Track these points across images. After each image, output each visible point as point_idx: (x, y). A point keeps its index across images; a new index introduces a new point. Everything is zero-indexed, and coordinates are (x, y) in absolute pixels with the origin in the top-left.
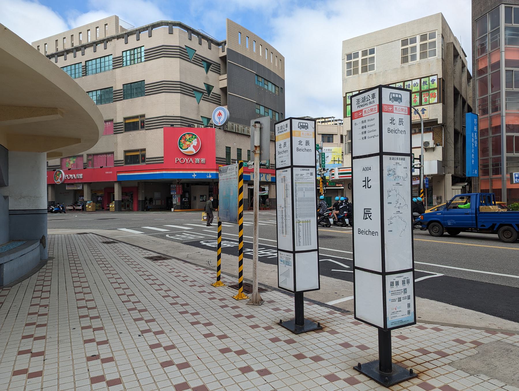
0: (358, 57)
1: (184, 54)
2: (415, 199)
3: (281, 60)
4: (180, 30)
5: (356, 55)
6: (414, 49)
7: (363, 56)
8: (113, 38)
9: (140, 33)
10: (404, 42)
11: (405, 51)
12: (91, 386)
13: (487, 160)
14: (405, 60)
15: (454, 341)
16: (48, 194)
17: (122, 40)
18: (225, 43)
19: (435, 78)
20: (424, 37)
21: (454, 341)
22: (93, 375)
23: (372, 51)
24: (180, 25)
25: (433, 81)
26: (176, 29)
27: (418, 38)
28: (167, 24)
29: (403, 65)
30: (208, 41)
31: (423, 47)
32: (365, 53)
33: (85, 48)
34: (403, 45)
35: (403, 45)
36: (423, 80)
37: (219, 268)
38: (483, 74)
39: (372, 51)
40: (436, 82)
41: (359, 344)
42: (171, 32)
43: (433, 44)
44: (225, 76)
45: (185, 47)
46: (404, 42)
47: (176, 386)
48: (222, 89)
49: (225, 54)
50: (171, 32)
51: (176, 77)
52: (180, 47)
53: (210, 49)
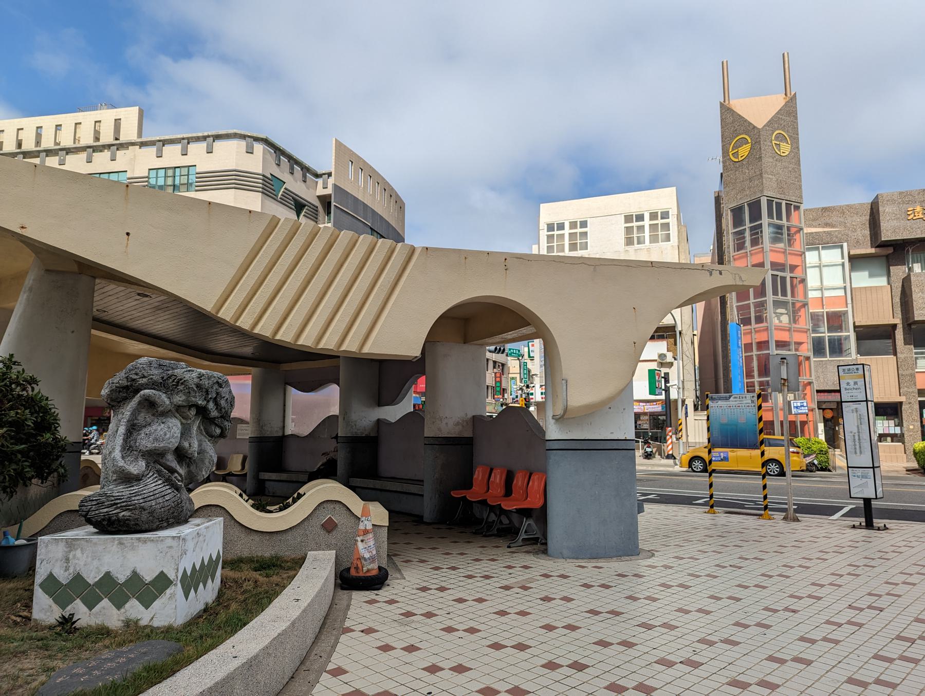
0: (563, 229)
1: (270, 187)
2: (751, 290)
3: (400, 206)
4: (264, 149)
5: (561, 226)
6: (641, 229)
7: (571, 228)
8: (133, 144)
9: (188, 143)
10: (628, 218)
11: (629, 230)
13: (748, 306)
17: (153, 150)
18: (330, 175)
20: (653, 216)
23: (584, 224)
24: (266, 141)
26: (259, 148)
28: (243, 137)
29: (628, 248)
30: (302, 169)
31: (653, 227)
32: (573, 225)
33: (67, 154)
34: (626, 222)
38: (824, 345)
39: (584, 224)
41: (544, 662)
42: (250, 151)
43: (666, 226)
45: (270, 176)
46: (628, 218)
49: (329, 191)
50: (250, 151)
52: (263, 176)
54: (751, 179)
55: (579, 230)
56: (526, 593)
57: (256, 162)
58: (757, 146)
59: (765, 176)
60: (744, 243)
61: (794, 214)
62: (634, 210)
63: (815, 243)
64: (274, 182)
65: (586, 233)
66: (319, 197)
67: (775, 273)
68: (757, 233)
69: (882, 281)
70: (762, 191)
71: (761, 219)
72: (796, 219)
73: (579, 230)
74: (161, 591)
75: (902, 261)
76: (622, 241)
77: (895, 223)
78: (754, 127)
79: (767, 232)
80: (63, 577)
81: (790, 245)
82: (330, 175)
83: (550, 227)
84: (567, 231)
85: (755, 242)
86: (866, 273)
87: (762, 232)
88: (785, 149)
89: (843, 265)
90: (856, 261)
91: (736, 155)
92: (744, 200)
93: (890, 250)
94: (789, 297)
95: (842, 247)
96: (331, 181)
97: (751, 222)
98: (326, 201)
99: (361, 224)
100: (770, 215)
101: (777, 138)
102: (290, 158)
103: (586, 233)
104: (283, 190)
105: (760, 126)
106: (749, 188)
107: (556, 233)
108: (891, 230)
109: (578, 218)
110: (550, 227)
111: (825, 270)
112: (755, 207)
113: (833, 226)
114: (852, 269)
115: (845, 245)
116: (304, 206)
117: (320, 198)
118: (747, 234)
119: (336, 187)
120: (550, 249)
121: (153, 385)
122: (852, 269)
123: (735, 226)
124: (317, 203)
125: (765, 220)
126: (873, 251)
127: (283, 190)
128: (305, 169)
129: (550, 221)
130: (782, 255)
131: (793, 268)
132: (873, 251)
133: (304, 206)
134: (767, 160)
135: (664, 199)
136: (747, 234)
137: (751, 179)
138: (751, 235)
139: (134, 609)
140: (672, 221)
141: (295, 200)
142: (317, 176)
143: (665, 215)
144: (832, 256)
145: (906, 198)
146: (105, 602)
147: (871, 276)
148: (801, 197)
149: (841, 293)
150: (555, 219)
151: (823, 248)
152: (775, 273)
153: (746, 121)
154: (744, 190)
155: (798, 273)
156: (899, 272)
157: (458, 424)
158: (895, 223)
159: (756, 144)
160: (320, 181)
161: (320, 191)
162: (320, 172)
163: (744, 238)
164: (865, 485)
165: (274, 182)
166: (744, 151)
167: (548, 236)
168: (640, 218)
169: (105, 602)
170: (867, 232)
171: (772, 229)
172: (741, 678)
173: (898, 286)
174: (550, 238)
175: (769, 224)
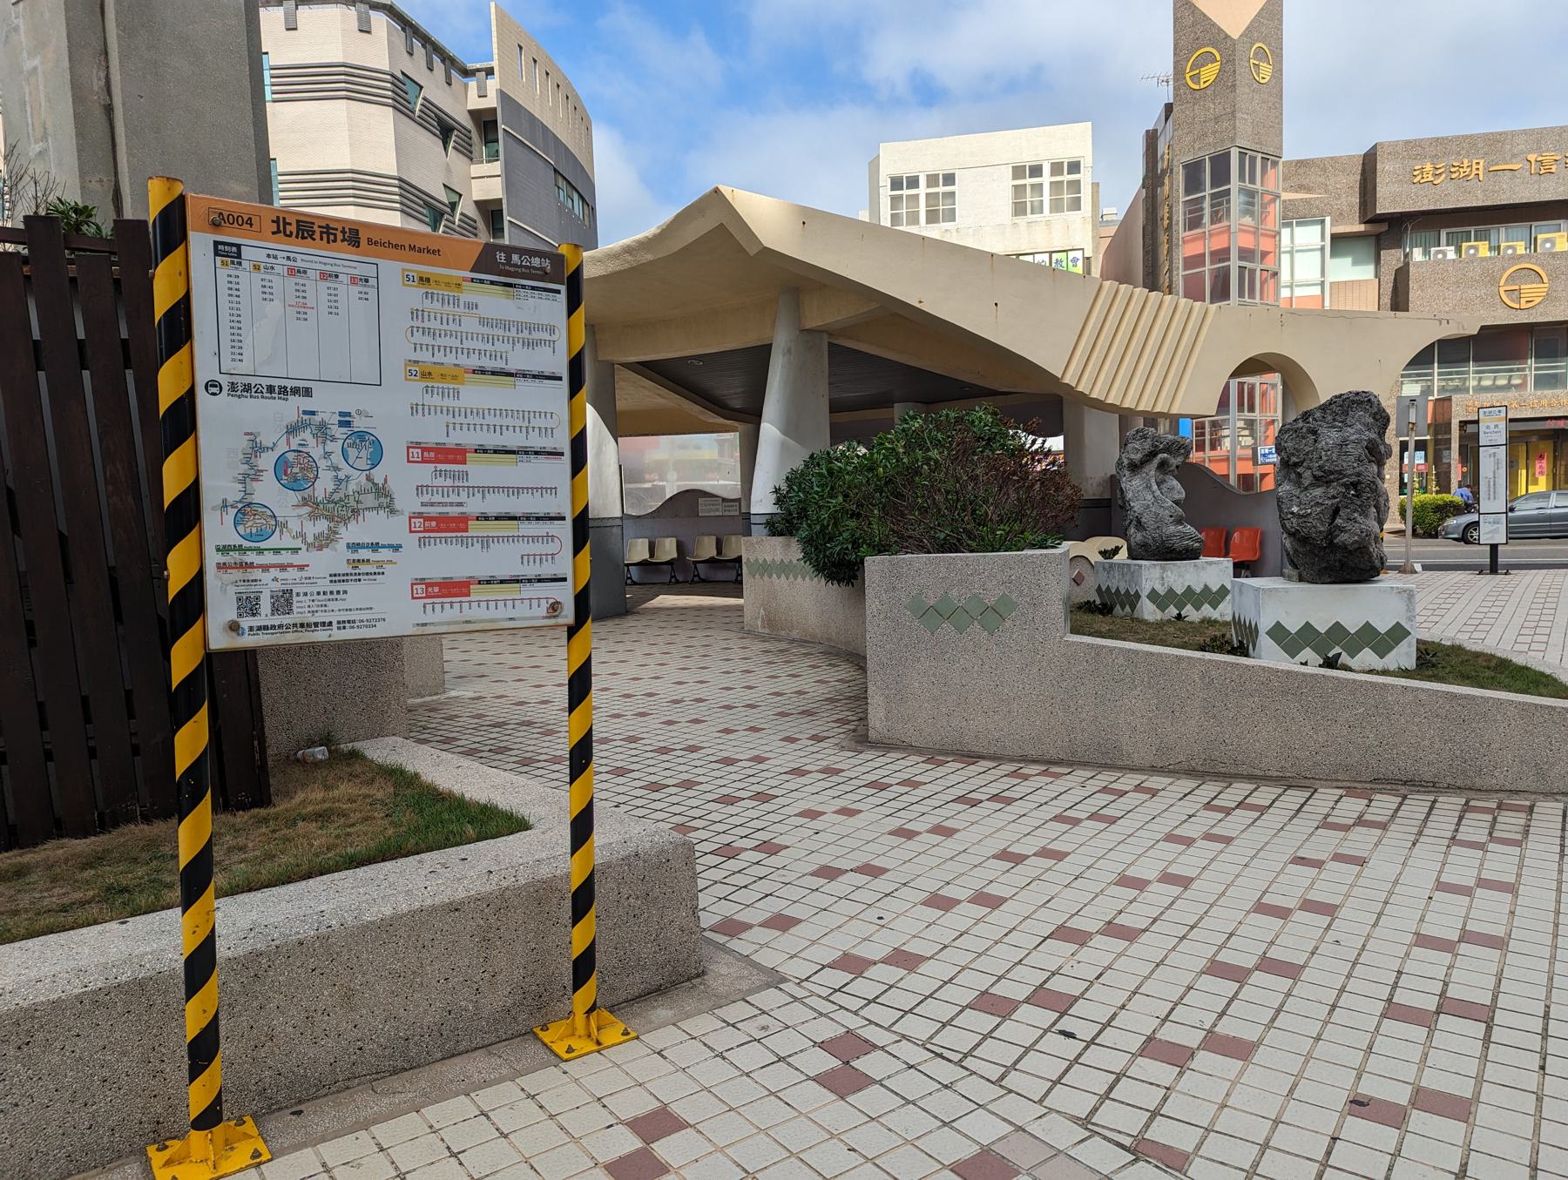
1: (401, 94)
5: (913, 182)
6: (1038, 188)
10: (1018, 172)
12: (1342, 1117)
14: (1019, 209)
15: (891, 833)
16: (449, 623)
19: (1079, 254)
21: (891, 833)
22: (1367, 1088)
23: (949, 179)
24: (391, 11)
25: (1075, 260)
26: (379, 20)
27: (1046, 169)
31: (1055, 186)
32: (932, 180)
34: (1015, 178)
35: (1015, 178)
36: (1055, 256)
37: (580, 757)
39: (949, 179)
40: (1080, 263)
43: (1075, 186)
44: (496, 167)
45: (400, 76)
46: (1018, 172)
47: (610, 1168)
48: (480, 205)
49: (491, 101)
51: (386, 163)
53: (449, 84)
54: (1217, 120)
55: (942, 189)
56: (756, 753)
57: (377, 49)
58: (1229, 67)
59: (1239, 115)
60: (1201, 217)
61: (1270, 172)
62: (1028, 159)
63: (1296, 216)
64: (409, 87)
65: (953, 194)
66: (470, 112)
67: (1243, 264)
68: (1220, 204)
69: (1366, 272)
70: (1233, 139)
71: (1228, 182)
72: (1272, 181)
73: (942, 189)
74: (1223, 598)
75: (1398, 244)
76: (1009, 209)
77: (1396, 188)
78: (1227, 36)
79: (1236, 200)
80: (1162, 591)
81: (1263, 221)
82: (490, 72)
83: (896, 183)
84: (922, 190)
85: (1215, 218)
86: (1349, 260)
87: (1228, 201)
88: (1266, 71)
89: (1322, 249)
90: (1340, 242)
91: (1196, 79)
92: (1206, 153)
93: (1384, 227)
94: (1257, 300)
95: (1323, 222)
96: (493, 84)
97: (1212, 186)
98: (486, 123)
99: (541, 163)
100: (1242, 177)
101: (1256, 53)
102: (426, 40)
103: (953, 194)
104: (420, 101)
105: (1235, 37)
106: (1214, 133)
107: (905, 192)
108: (1389, 201)
109: (941, 168)
110: (896, 183)
111: (1297, 256)
112: (1221, 165)
113: (1309, 190)
114: (1334, 254)
115: (1328, 219)
116: (452, 129)
117: (474, 114)
118: (1207, 204)
119: (503, 95)
120: (895, 219)
121: (1167, 450)
122: (1334, 254)
123: (1188, 192)
124: (467, 122)
125: (1234, 184)
126: (1362, 228)
127: (420, 101)
128: (449, 61)
129: (896, 172)
130: (1251, 237)
131: (1264, 254)
132: (1362, 228)
133: (452, 129)
134: (1243, 90)
135: (1071, 140)
136: (1207, 204)
137: (1217, 120)
138: (1212, 206)
139: (1207, 611)
140: (1085, 177)
141: (441, 122)
142: (467, 73)
143: (1075, 167)
144: (1310, 236)
145: (1414, 149)
146: (1206, 606)
147: (1355, 263)
148: (1281, 148)
149: (1316, 291)
150: (904, 170)
151: (1299, 224)
152: (1243, 264)
153: (1214, 25)
154: (1205, 135)
155: (1269, 264)
156: (1392, 258)
157: (1099, 485)
158: (1396, 188)
159: (1229, 62)
160: (473, 84)
161: (475, 103)
162: (471, 66)
163: (1202, 209)
164: (1496, 531)
165: (409, 87)
166: (1209, 73)
167: (893, 198)
168: (1036, 171)
169: (1206, 606)
170: (1356, 200)
171: (1243, 198)
172: (1054, 846)
173: (1388, 280)
174: (895, 201)
175: (1241, 190)
